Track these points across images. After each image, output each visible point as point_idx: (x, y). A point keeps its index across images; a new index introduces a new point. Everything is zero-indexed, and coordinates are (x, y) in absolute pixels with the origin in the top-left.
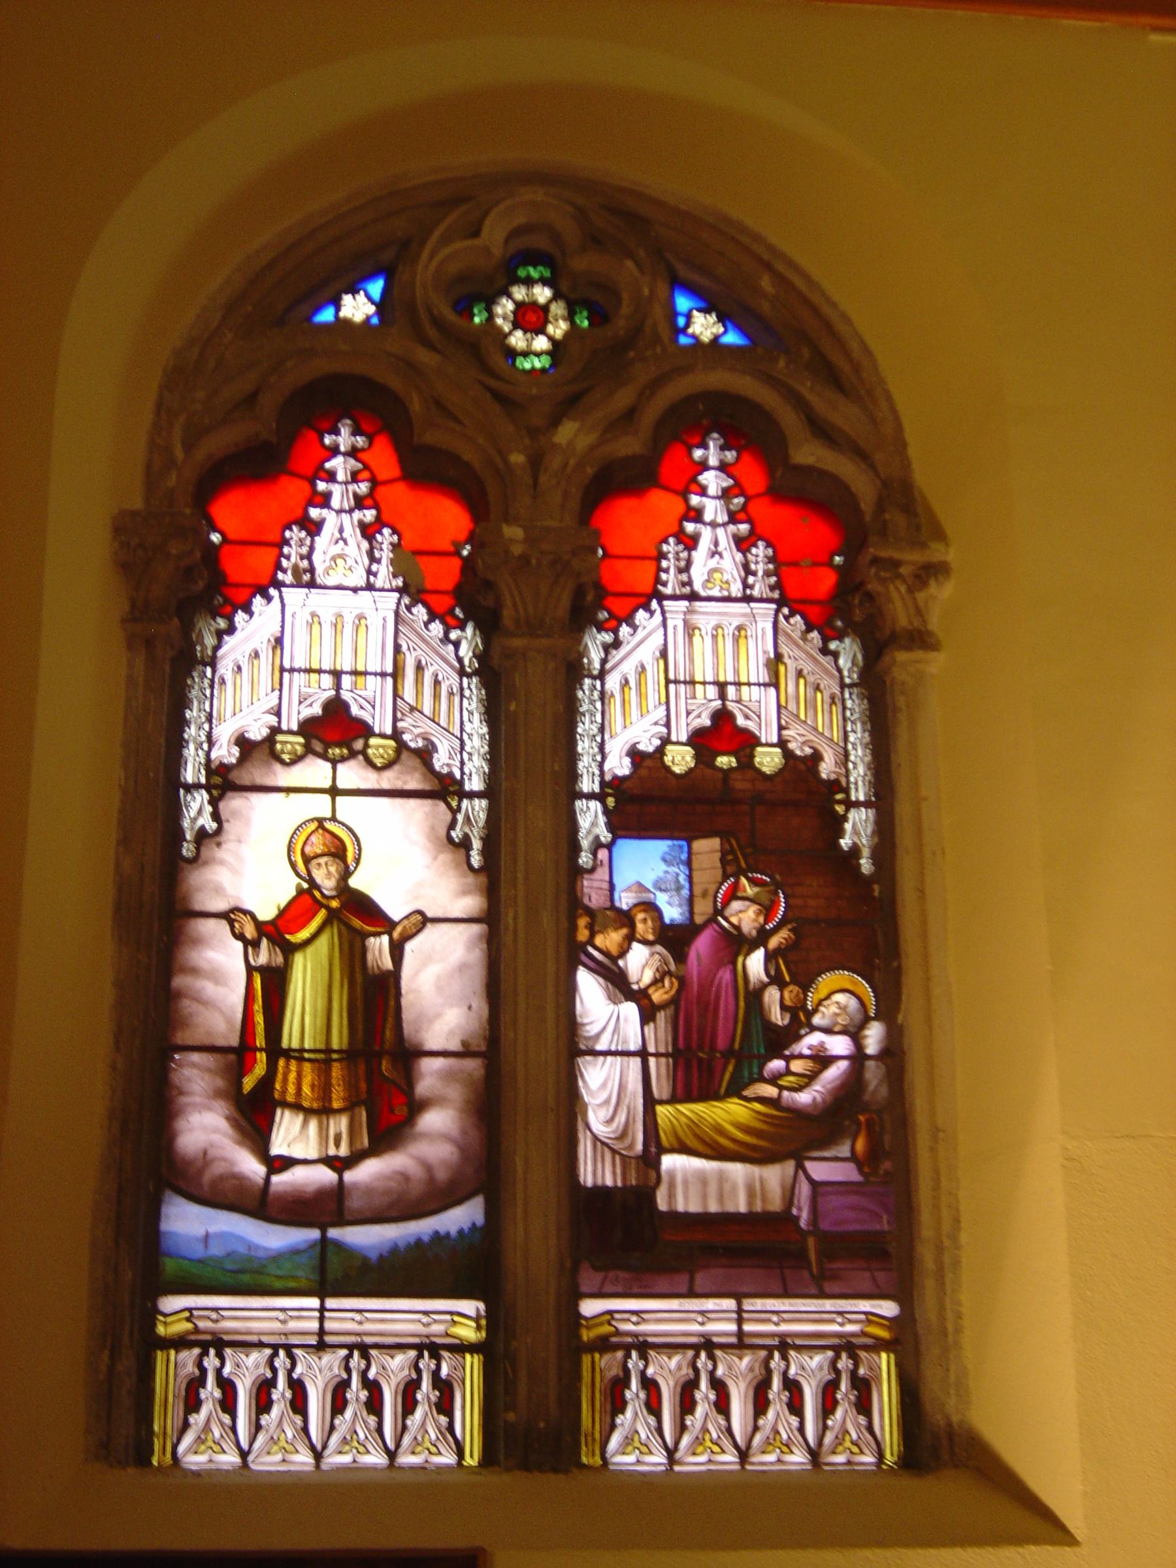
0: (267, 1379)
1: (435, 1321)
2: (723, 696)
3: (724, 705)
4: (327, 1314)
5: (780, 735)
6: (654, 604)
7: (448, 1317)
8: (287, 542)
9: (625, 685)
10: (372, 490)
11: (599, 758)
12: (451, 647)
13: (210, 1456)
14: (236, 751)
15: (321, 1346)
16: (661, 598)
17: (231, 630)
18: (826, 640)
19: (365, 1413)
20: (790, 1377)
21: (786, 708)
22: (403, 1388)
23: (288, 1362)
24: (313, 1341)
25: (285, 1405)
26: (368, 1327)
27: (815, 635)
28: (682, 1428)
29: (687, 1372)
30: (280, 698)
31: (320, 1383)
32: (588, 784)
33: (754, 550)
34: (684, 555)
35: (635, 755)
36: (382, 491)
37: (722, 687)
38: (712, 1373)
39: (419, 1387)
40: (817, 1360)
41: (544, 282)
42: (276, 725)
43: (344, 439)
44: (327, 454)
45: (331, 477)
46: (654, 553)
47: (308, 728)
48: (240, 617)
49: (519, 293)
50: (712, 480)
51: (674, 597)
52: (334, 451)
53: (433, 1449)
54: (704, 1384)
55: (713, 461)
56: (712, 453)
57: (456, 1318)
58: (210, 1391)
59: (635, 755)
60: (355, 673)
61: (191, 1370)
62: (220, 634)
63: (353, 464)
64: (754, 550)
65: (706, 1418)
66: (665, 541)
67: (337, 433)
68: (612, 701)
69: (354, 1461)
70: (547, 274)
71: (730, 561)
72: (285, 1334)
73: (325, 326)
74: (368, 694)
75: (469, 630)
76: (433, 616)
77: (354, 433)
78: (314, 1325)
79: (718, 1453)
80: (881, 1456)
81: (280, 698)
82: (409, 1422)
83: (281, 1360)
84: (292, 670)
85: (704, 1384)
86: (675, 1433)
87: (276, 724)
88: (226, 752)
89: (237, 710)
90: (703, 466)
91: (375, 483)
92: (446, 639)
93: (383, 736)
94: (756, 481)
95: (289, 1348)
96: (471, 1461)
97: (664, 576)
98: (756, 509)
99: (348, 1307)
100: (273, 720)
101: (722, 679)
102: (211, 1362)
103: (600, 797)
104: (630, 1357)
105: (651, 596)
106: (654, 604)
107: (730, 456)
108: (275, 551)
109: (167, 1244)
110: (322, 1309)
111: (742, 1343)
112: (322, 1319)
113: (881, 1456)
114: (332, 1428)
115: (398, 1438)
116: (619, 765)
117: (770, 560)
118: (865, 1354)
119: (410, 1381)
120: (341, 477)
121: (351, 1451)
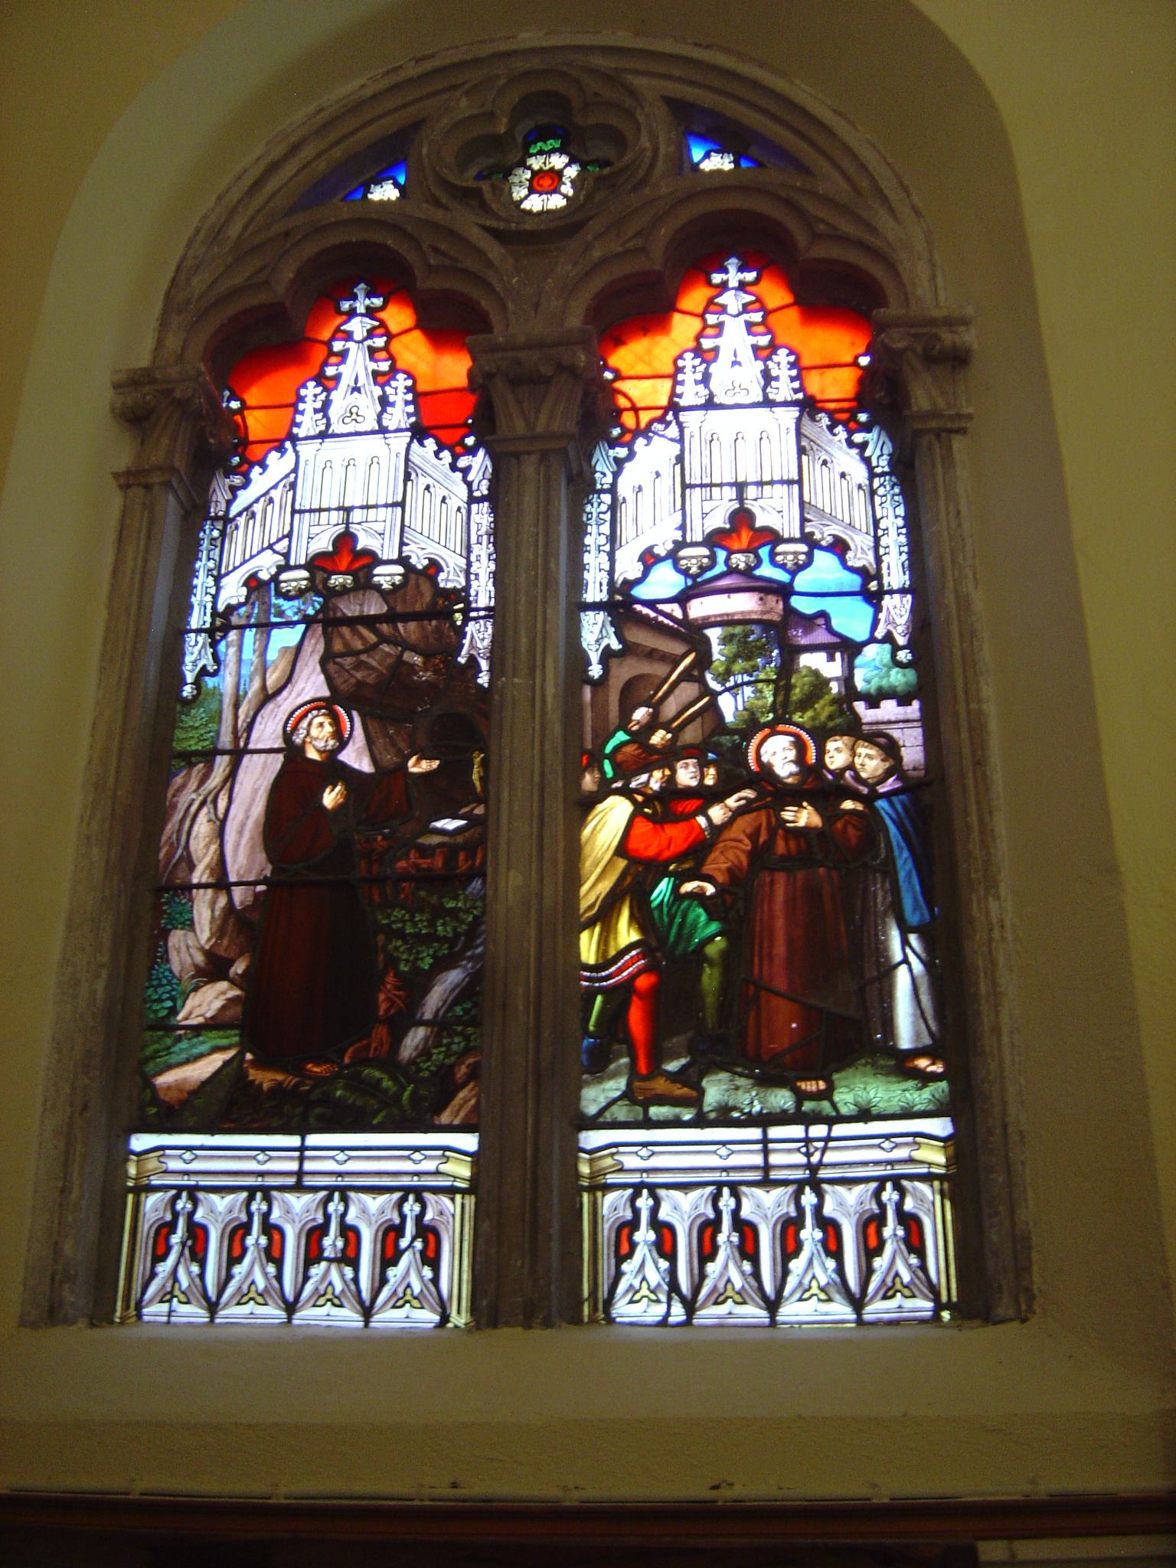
1: (426, 1157)
2: (740, 498)
3: (347, 528)
4: (771, 1146)
5: (400, 552)
8: (302, 399)
9: (251, 518)
10: (387, 343)
11: (213, 591)
12: (459, 475)
17: (631, 455)
18: (455, 457)
21: (810, 503)
23: (651, 1202)
26: (351, 1166)
27: (840, 429)
28: (867, 1273)
32: (595, 593)
33: (393, 383)
34: (323, 397)
36: (773, 319)
41: (561, 151)
42: (680, 539)
43: (734, 276)
45: (348, 336)
49: (536, 163)
52: (352, 313)
55: (361, 309)
57: (918, 1139)
58: (810, 1235)
60: (760, 484)
62: (619, 463)
63: (370, 323)
66: (304, 386)
70: (557, 144)
76: (441, 447)
84: (301, 512)
87: (680, 539)
88: (233, 591)
91: (767, 313)
92: (453, 467)
93: (790, 540)
95: (652, 1188)
96: (459, 1319)
97: (299, 418)
99: (905, 1130)
100: (678, 536)
102: (644, 1203)
107: (750, 276)
108: (291, 410)
109: (158, 1087)
115: (778, 1282)
117: (792, 365)
120: (358, 336)
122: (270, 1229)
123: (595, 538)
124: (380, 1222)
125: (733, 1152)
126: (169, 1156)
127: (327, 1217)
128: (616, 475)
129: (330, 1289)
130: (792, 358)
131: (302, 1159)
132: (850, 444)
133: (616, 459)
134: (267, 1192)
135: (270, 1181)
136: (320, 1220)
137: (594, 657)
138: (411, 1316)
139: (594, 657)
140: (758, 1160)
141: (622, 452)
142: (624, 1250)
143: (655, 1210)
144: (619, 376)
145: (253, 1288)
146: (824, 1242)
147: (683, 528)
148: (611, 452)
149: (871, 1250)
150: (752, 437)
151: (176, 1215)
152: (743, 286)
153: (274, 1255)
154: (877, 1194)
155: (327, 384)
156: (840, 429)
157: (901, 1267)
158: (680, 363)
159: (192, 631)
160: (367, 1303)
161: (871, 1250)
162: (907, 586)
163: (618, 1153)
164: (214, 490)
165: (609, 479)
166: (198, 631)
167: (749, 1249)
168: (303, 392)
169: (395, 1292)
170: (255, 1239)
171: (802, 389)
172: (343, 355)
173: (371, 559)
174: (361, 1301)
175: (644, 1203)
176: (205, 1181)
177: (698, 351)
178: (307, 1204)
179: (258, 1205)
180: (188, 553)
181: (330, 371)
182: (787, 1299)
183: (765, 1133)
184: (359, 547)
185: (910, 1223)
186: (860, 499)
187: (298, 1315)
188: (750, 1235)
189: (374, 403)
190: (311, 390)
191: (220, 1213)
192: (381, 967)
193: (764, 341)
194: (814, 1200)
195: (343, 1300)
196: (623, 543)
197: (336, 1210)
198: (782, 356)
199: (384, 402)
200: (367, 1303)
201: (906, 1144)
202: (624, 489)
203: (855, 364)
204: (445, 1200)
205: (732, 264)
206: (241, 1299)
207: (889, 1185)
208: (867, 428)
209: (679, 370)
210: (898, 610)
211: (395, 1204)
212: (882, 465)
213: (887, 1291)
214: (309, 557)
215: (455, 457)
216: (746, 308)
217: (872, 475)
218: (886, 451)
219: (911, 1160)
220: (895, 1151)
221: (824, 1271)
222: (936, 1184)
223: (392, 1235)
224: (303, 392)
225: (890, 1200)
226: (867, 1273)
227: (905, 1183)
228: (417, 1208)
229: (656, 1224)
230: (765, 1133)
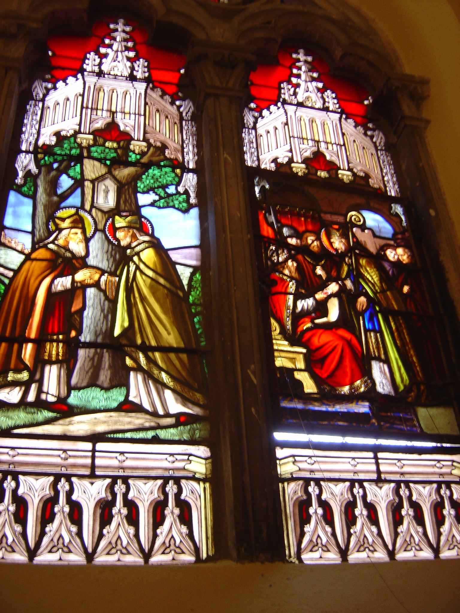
0: (350, 501)
6: (79, 76)
13: (414, 553)
14: (54, 139)
15: (93, 476)
19: (69, 523)
24: (87, 472)
25: (364, 519)
29: (348, 496)
31: (428, 505)
33: (138, 62)
37: (113, 113)
38: (451, 497)
48: (60, 84)
53: (124, 551)
54: (406, 504)
58: (315, 510)
61: (392, 498)
62: (48, 90)
64: (138, 62)
65: (61, 523)
67: (117, 24)
68: (48, 111)
72: (355, 473)
77: (125, 25)
78: (89, 461)
79: (449, 547)
80: (197, 550)
82: (442, 530)
83: (120, 488)
85: (406, 504)
86: (435, 535)
89: (56, 122)
90: (298, 60)
95: (68, 477)
100: (77, 128)
104: (401, 487)
106: (79, 76)
110: (94, 451)
112: (93, 457)
113: (197, 550)
114: (101, 536)
115: (94, 544)
120: (118, 39)
121: (412, 549)
125: (18, 454)
129: (172, 542)
133: (46, 88)
137: (21, 174)
138: (121, 559)
139: (21, 174)
143: (70, 492)
144: (252, 84)
146: (369, 517)
147: (80, 125)
148: (44, 84)
149: (439, 521)
152: (124, 31)
154: (163, 488)
157: (174, 533)
159: (23, 152)
160: (90, 550)
164: (36, 87)
166: (27, 152)
169: (110, 543)
173: (127, 138)
174: (430, 545)
175: (171, 488)
180: (21, 113)
182: (303, 552)
183: (94, 447)
189: (319, 100)
195: (328, 547)
196: (46, 125)
200: (90, 550)
202: (261, 131)
204: (194, 484)
207: (119, 481)
213: (360, 547)
214: (303, 159)
218: (191, 110)
219: (184, 469)
222: (201, 483)
224: (88, 56)
227: (411, 485)
228: (13, 484)
230: (94, 447)
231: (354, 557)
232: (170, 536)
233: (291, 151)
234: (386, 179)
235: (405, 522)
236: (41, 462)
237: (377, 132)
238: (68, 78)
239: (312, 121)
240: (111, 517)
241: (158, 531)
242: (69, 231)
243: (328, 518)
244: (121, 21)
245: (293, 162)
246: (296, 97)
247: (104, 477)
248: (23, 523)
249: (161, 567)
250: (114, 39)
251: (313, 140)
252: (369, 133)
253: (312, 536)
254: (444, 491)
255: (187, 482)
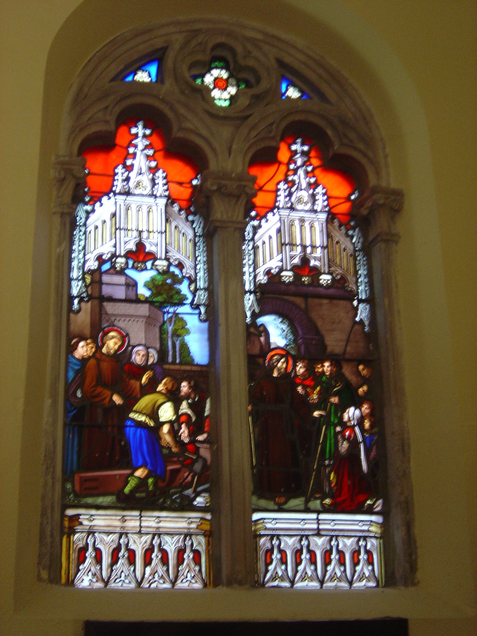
5: (166, 256)
7: (368, 523)
8: (116, 174)
16: (279, 208)
17: (93, 211)
18: (347, 230)
20: (281, 548)
22: (136, 553)
28: (325, 571)
29: (355, 547)
30: (282, 256)
35: (268, 273)
39: (185, 552)
40: (349, 542)
44: (133, 137)
46: (111, 173)
47: (129, 255)
50: (141, 143)
51: (120, 194)
54: (305, 551)
56: (139, 130)
59: (268, 273)
62: (88, 213)
69: (157, 586)
71: (146, 179)
73: (129, 82)
74: (155, 241)
75: (357, 230)
81: (282, 256)
90: (136, 136)
94: (158, 144)
95: (278, 536)
98: (317, 172)
101: (140, 229)
103: (254, 292)
105: (109, 191)
108: (111, 179)
111: (318, 533)
116: (262, 279)
118: (131, 536)
119: (181, 549)
122: (310, 552)
123: (248, 261)
124: (352, 549)
126: (267, 523)
127: (331, 547)
128: (87, 218)
130: (324, 191)
131: (319, 524)
132: (347, 235)
134: (307, 536)
135: (307, 533)
136: (328, 548)
137: (249, 314)
140: (315, 526)
141: (89, 208)
142: (82, 559)
145: (306, 576)
150: (145, 209)
151: (360, 547)
152: (145, 136)
153: (342, 562)
155: (130, 168)
156: (182, 212)
158: (279, 187)
160: (139, 580)
161: (356, 563)
162: (252, 290)
163: (263, 522)
165: (83, 220)
167: (313, 560)
168: (116, 171)
170: (305, 556)
171: (167, 190)
172: (134, 155)
176: (341, 533)
177: (286, 181)
178: (294, 541)
179: (362, 543)
181: (129, 162)
184: (147, 250)
185: (369, 553)
186: (190, 246)
187: (324, 585)
188: (284, 555)
190: (120, 170)
191: (290, 546)
192: (374, 448)
193: (313, 180)
194: (277, 543)
197: (124, 542)
198: (319, 190)
199: (313, 197)
200: (139, 580)
201: (367, 525)
203: (348, 199)
205: (140, 125)
206: (303, 579)
208: (354, 228)
209: (278, 190)
210: (202, 296)
211: (328, 541)
212: (199, 231)
215: (347, 230)
216: (146, 147)
217: (195, 236)
220: (363, 526)
221: (161, 570)
223: (269, 554)
225: (334, 545)
226: (325, 571)
229: (310, 552)
231: (299, 585)
232: (276, 572)
233: (115, 246)
234: (198, 267)
235: (333, 563)
236: (291, 528)
237: (197, 217)
238: (102, 198)
239: (302, 221)
240: (85, 558)
241: (81, 567)
242: (157, 349)
243: (313, 561)
244: (140, 125)
245: (117, 257)
246: (128, 183)
247: (147, 534)
248: (373, 565)
249: (329, 591)
250: (136, 146)
251: (137, 230)
252: (191, 218)
253: (303, 572)
254: (333, 543)
255: (99, 535)
